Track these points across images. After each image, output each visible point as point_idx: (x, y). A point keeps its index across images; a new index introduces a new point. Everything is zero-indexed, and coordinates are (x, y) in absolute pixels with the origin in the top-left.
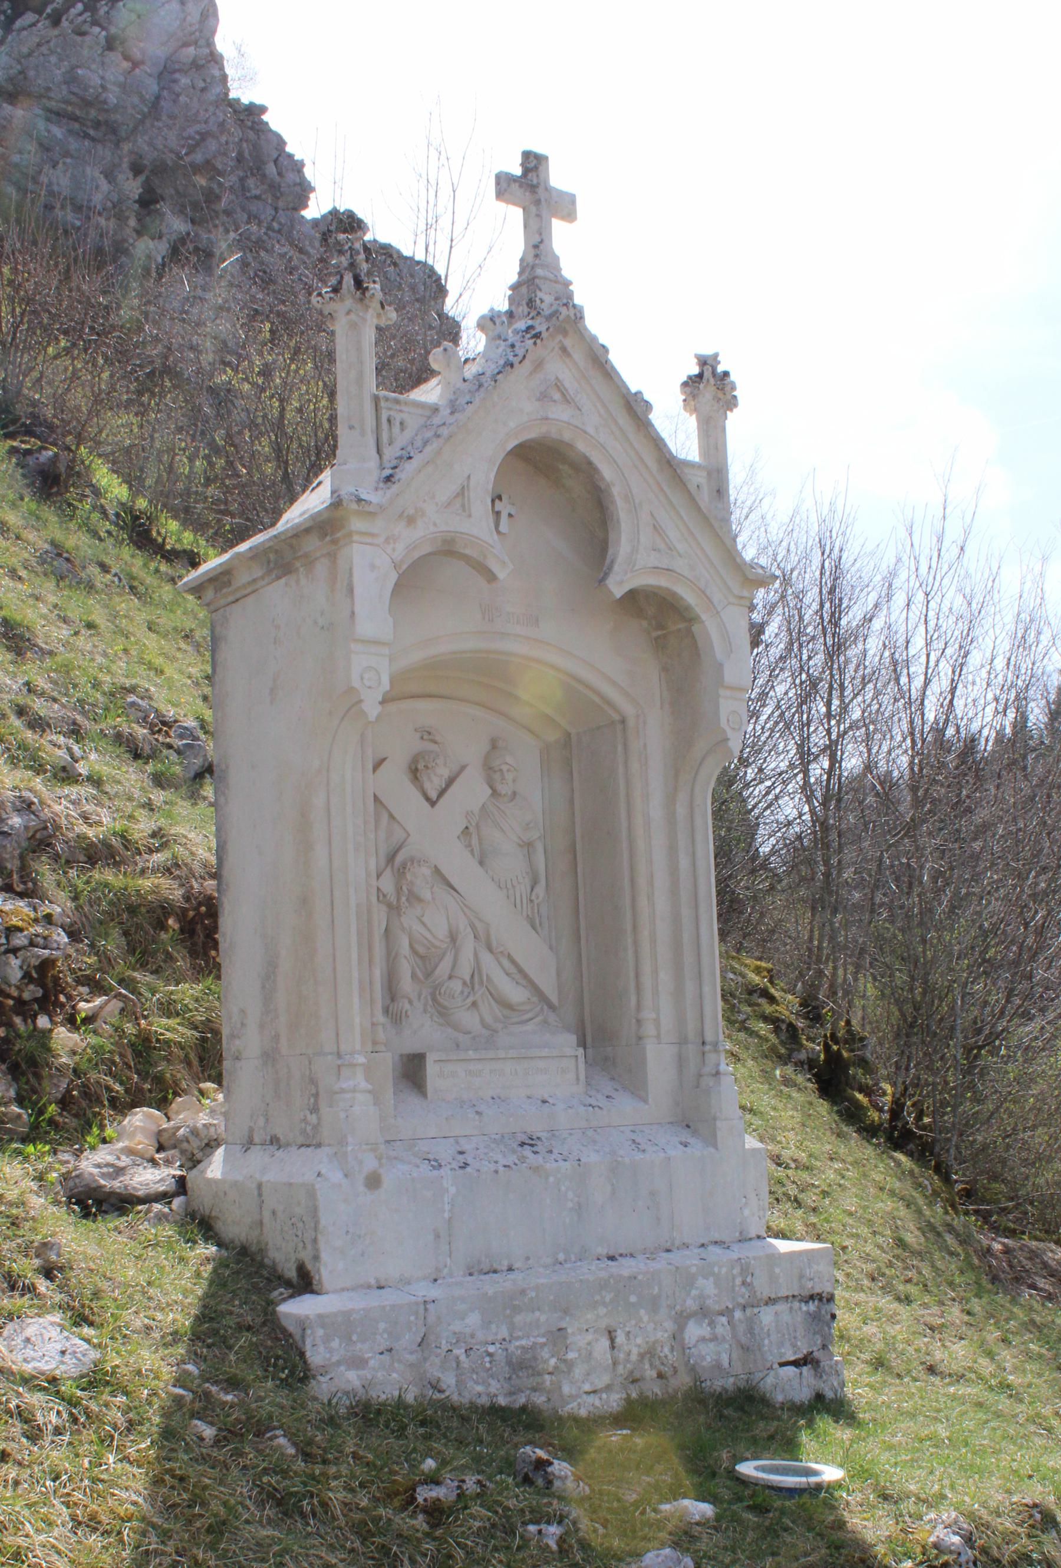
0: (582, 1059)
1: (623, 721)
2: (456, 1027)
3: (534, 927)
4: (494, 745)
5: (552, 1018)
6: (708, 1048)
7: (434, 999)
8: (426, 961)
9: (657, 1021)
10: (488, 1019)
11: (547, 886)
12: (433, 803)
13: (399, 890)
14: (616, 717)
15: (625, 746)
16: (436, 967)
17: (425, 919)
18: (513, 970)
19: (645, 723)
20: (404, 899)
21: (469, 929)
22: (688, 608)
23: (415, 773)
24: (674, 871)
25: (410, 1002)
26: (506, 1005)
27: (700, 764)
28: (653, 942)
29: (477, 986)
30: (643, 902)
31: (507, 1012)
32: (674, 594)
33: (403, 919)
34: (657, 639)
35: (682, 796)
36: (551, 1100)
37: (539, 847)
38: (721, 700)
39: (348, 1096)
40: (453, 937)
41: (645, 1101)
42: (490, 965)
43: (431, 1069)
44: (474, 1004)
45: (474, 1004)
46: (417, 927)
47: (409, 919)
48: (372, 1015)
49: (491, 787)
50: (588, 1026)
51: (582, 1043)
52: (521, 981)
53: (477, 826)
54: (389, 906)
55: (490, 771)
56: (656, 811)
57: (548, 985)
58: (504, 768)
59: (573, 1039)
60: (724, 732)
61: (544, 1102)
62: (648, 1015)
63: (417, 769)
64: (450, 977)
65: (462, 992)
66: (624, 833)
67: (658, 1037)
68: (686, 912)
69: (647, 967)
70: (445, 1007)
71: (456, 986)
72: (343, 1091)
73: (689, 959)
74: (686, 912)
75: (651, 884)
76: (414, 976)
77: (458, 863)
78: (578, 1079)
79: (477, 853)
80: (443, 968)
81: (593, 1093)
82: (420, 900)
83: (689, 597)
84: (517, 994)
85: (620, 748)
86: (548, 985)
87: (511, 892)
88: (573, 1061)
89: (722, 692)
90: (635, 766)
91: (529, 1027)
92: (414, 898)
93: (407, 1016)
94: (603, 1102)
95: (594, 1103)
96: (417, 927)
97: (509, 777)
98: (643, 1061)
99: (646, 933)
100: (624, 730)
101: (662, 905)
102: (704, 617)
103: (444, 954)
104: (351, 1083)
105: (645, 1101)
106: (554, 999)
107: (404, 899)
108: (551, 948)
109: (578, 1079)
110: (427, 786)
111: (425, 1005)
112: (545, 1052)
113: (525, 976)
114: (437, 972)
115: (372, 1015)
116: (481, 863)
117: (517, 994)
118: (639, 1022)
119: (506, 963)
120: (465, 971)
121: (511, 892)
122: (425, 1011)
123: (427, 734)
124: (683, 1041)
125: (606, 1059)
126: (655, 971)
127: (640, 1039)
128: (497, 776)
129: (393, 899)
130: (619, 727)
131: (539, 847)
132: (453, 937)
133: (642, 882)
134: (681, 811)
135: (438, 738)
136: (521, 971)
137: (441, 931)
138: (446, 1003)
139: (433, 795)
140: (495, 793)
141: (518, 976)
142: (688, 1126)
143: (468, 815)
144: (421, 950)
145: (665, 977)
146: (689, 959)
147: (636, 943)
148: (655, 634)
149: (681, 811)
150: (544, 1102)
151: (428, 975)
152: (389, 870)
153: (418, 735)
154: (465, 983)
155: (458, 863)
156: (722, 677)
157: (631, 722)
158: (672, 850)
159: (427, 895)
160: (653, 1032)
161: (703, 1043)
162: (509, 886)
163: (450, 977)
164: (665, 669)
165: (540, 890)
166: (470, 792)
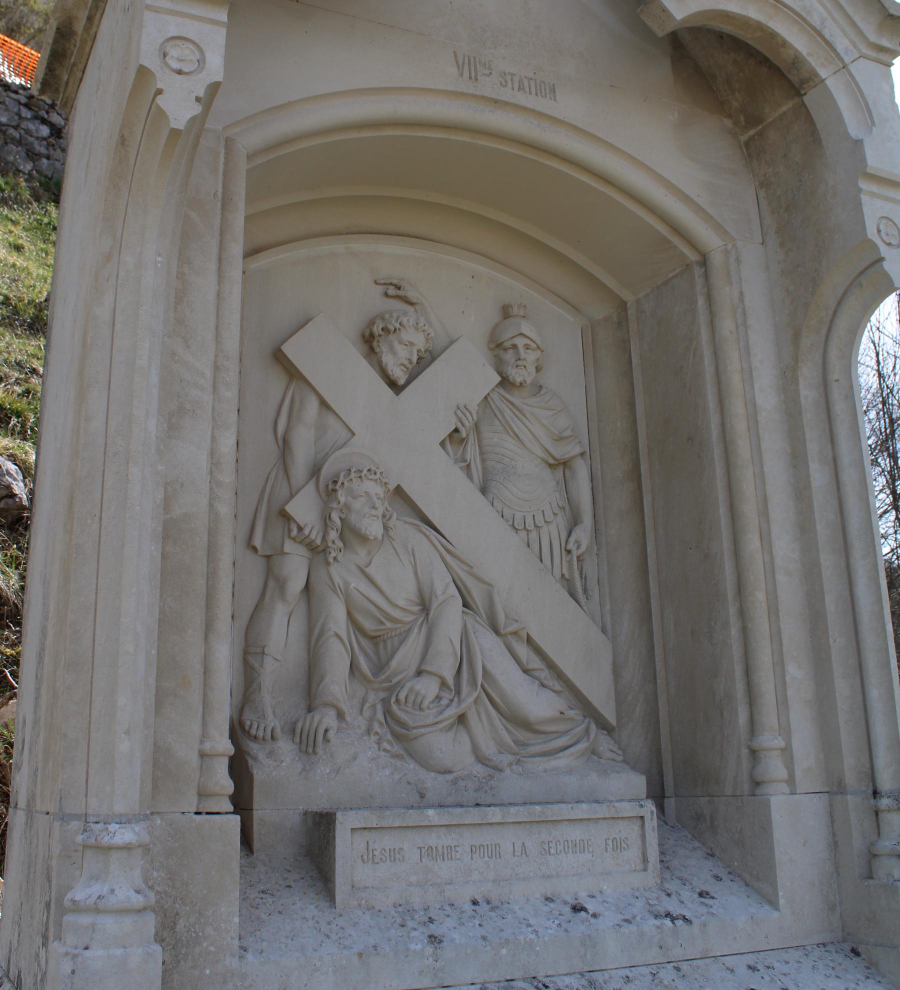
0: (652, 823)
1: (704, 262)
2: (424, 763)
3: (573, 595)
4: (506, 312)
5: (605, 744)
6: (885, 802)
7: (388, 712)
8: (376, 642)
9: (787, 752)
10: (489, 748)
11: (596, 530)
12: (395, 387)
13: (326, 520)
14: (692, 256)
15: (709, 297)
16: (391, 657)
17: (371, 570)
18: (536, 663)
19: (738, 261)
20: (333, 535)
21: (453, 590)
22: (797, 61)
23: (369, 342)
24: (801, 492)
25: (340, 715)
26: (518, 721)
27: (835, 312)
28: (773, 611)
29: (465, 689)
30: (752, 543)
31: (522, 735)
32: (772, 35)
33: (334, 570)
34: (747, 144)
35: (808, 374)
36: (591, 906)
37: (582, 470)
38: (864, 198)
39: (85, 920)
40: (424, 605)
41: (773, 904)
42: (489, 650)
43: (346, 846)
44: (462, 719)
45: (462, 719)
46: (358, 584)
47: (343, 571)
48: (204, 736)
49: (500, 373)
50: (667, 758)
51: (657, 794)
52: (550, 682)
53: (477, 426)
54: (312, 548)
55: (498, 348)
56: (767, 399)
57: (599, 691)
58: (520, 342)
59: (638, 783)
60: (875, 247)
61: (578, 909)
62: (770, 740)
63: (372, 335)
64: (419, 673)
65: (438, 698)
66: (715, 433)
67: (791, 781)
68: (828, 561)
69: (764, 657)
70: (403, 725)
71: (428, 688)
72: (77, 908)
73: (838, 642)
74: (828, 561)
75: (764, 513)
76: (353, 667)
77: (440, 485)
78: (645, 860)
79: (477, 473)
80: (406, 656)
81: (672, 886)
82: (364, 539)
83: (798, 41)
84: (538, 704)
85: (701, 302)
86: (599, 691)
87: (534, 535)
88: (636, 827)
89: (863, 185)
90: (727, 325)
91: (562, 761)
92: (351, 534)
93: (326, 740)
94: (691, 907)
95: (676, 910)
96: (358, 584)
97: (531, 357)
98: (766, 828)
99: (760, 596)
100: (706, 276)
101: (785, 547)
102: (823, 73)
103: (409, 631)
104: (96, 889)
105: (773, 904)
106: (609, 714)
107: (333, 535)
108: (604, 630)
109: (645, 860)
110: (388, 360)
111: (371, 720)
112: (583, 810)
113: (560, 675)
114: (394, 663)
115: (204, 736)
116: (484, 490)
117: (538, 704)
118: (754, 753)
119: (523, 651)
120: (445, 664)
121: (534, 535)
122: (369, 731)
123: (394, 290)
124: (835, 789)
125: (699, 817)
126: (780, 665)
127: (757, 783)
128: (509, 356)
129: (316, 536)
130: (698, 271)
131: (582, 470)
132: (424, 605)
133: (749, 509)
134: (808, 394)
135: (412, 295)
136: (551, 665)
137: (403, 593)
138: (403, 717)
139: (400, 376)
140: (505, 382)
141: (545, 674)
142: (855, 952)
143: (460, 410)
144: (368, 625)
145: (797, 673)
146: (838, 642)
147: (742, 613)
148: (744, 138)
149: (808, 394)
150: (578, 909)
151: (380, 667)
152: (311, 486)
153: (380, 289)
154: (443, 684)
155: (440, 485)
156: (863, 160)
157: (717, 259)
158: (797, 459)
159: (374, 529)
160: (782, 773)
161: (876, 793)
162: (530, 525)
163: (419, 673)
164: (764, 184)
165: (583, 535)
166: (464, 377)
